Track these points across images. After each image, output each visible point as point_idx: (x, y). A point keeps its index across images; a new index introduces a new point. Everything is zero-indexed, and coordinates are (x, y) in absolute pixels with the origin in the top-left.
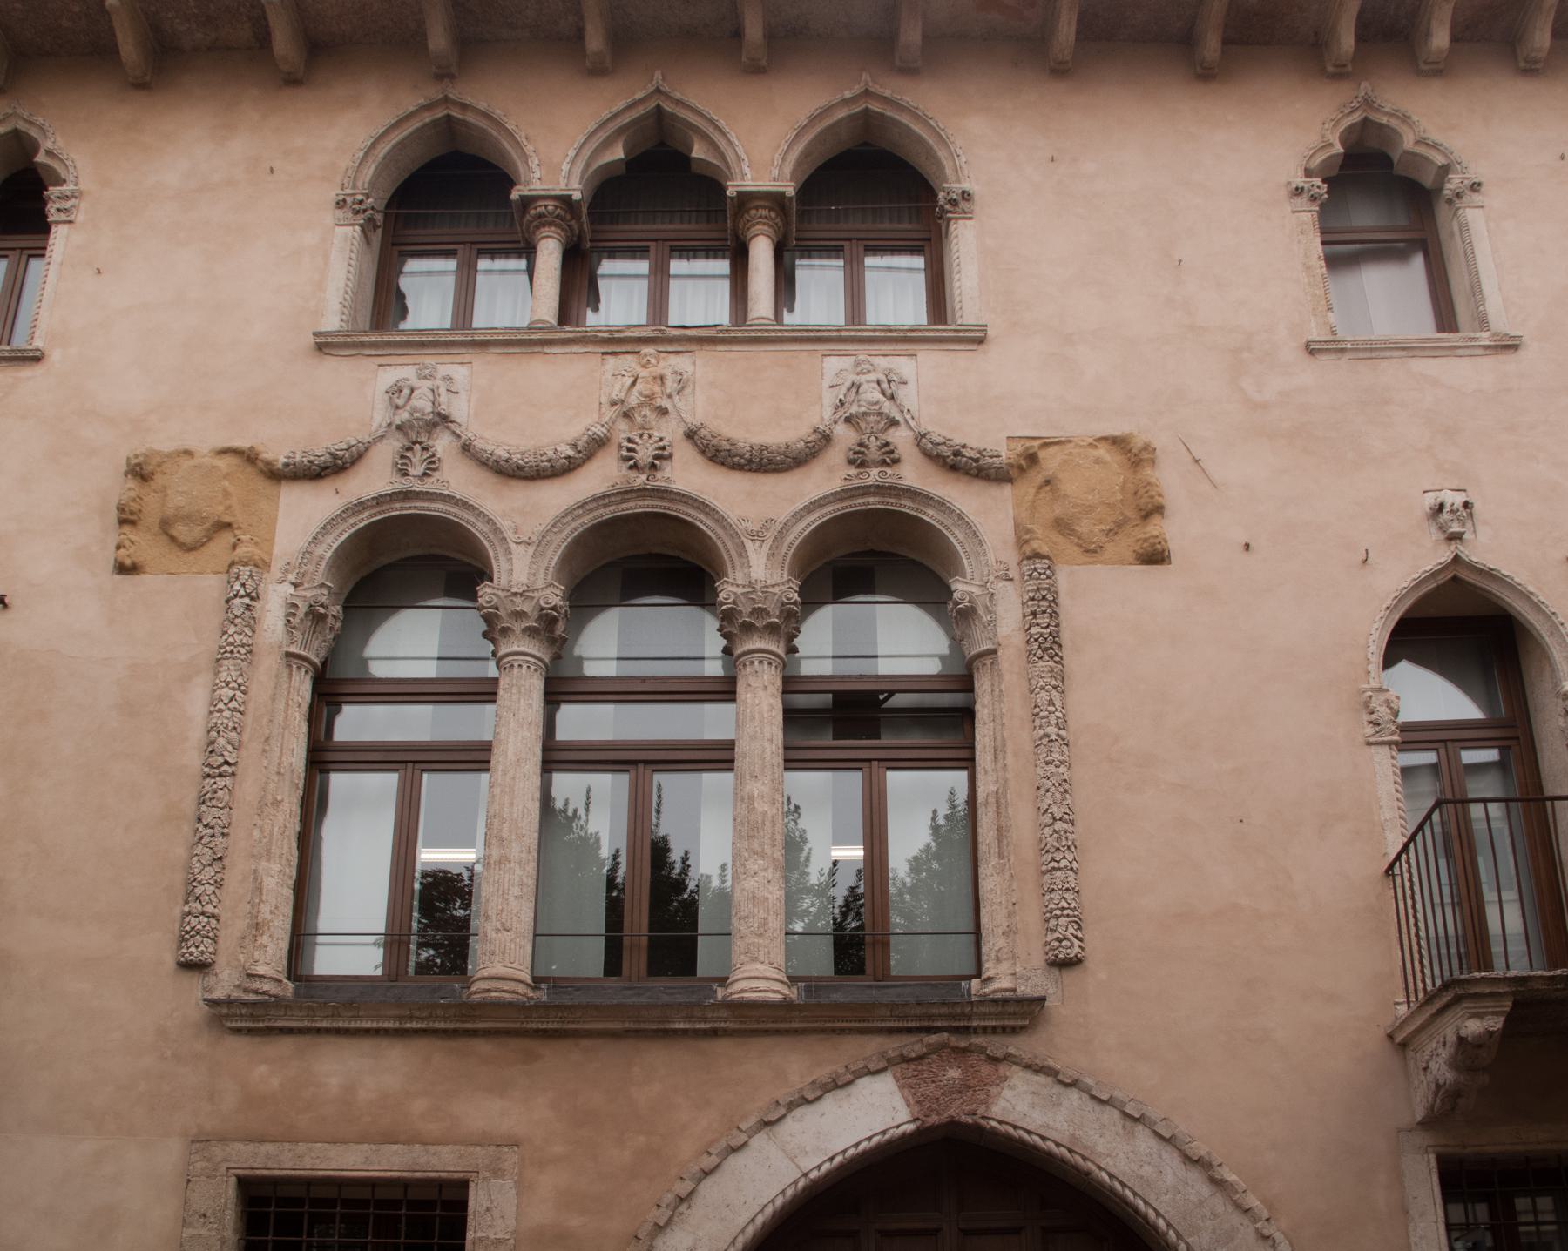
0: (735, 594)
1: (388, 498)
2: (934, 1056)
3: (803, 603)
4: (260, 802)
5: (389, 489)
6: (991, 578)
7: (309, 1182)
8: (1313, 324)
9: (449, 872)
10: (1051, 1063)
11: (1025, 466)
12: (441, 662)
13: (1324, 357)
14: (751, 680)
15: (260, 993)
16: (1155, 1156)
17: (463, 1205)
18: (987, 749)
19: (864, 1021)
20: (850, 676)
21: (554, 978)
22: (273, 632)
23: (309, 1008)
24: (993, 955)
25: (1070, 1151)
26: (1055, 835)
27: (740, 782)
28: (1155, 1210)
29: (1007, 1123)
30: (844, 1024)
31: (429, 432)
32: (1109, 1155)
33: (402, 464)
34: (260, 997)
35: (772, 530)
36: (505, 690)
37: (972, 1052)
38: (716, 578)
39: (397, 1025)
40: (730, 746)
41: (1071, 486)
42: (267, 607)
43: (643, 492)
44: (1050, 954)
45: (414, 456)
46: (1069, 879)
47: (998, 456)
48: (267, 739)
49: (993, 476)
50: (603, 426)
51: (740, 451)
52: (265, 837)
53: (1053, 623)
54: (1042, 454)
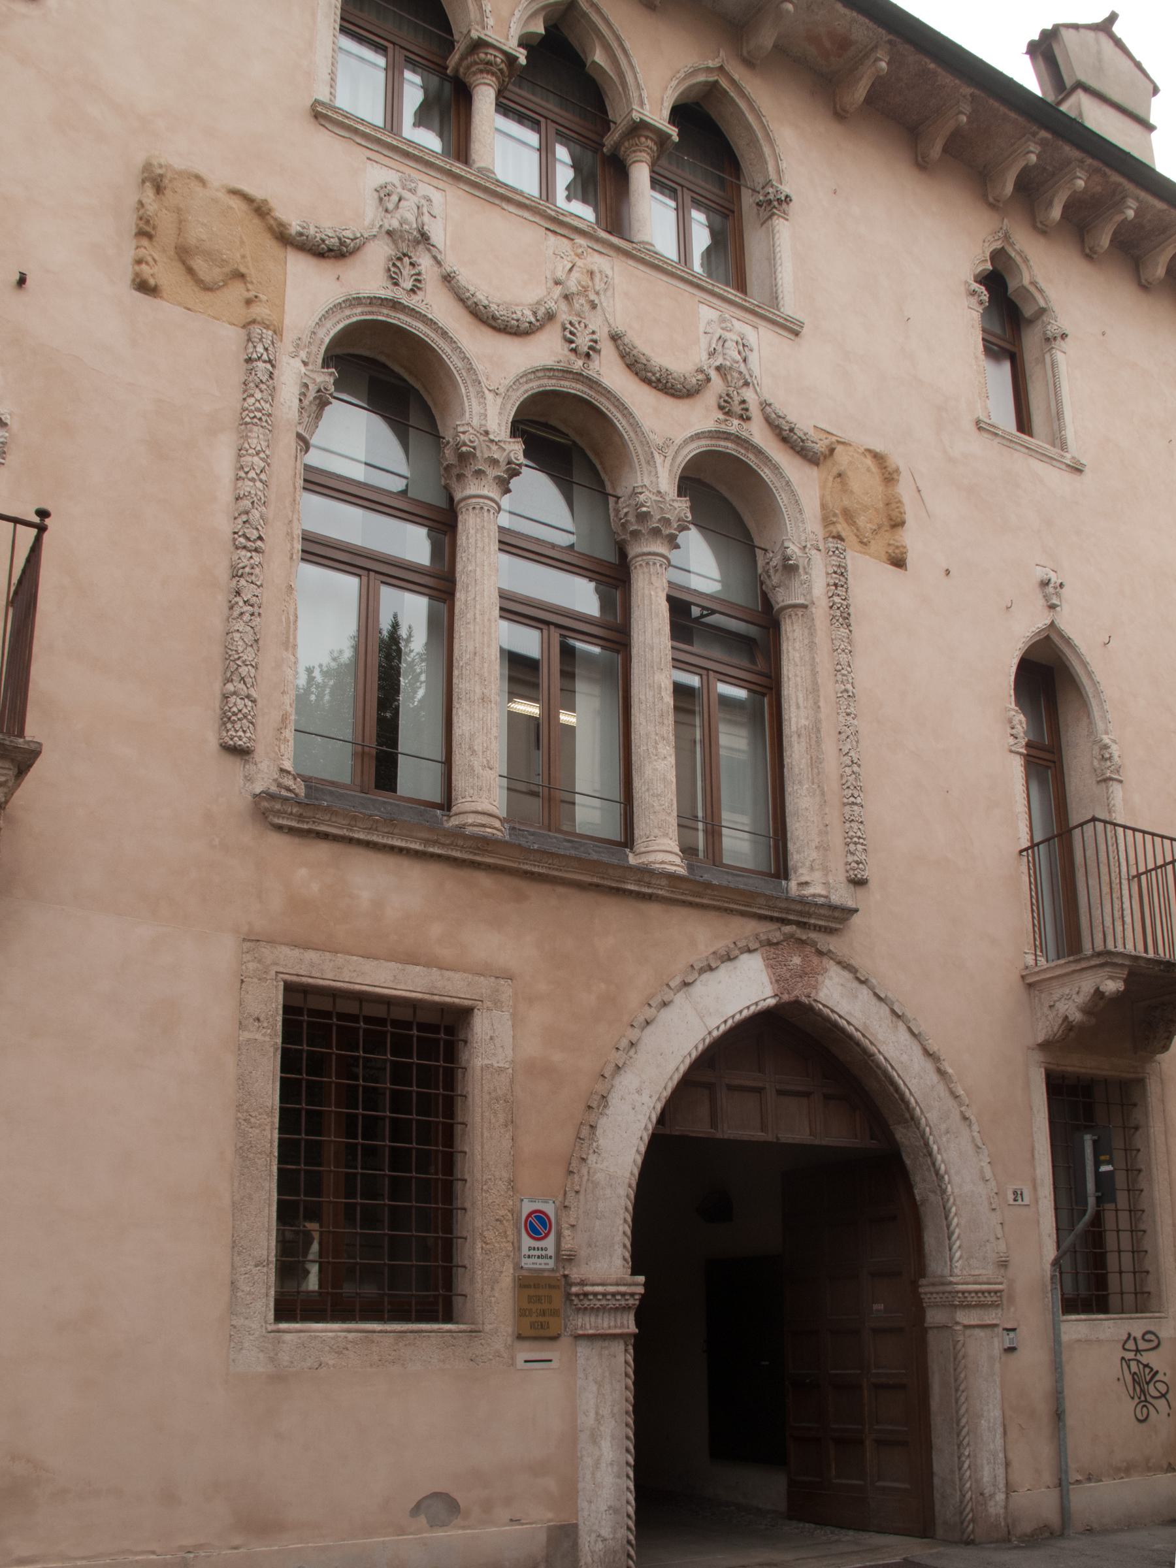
1: (380, 302)
2: (785, 944)
7: (334, 994)
8: (979, 406)
10: (852, 962)
13: (986, 435)
23: (354, 818)
24: (808, 864)
29: (828, 1007)
30: (735, 907)
32: (884, 1042)
45: (404, 267)
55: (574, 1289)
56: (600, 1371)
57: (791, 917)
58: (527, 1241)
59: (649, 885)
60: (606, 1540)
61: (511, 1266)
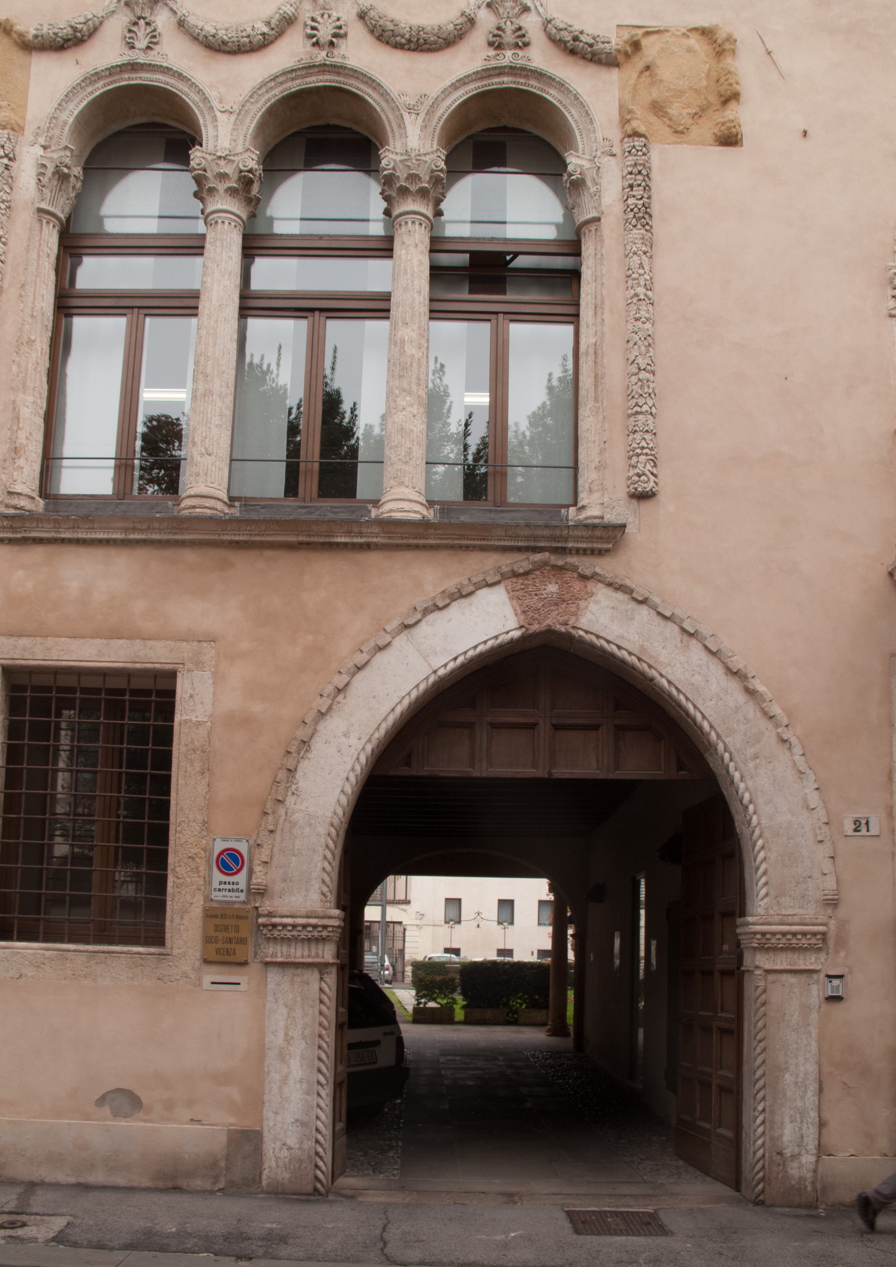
0: (394, 161)
1: (119, 69)
2: (538, 573)
3: (448, 172)
4: (17, 341)
5: (119, 61)
6: (599, 153)
7: (56, 672)
9: (170, 417)
10: (628, 582)
11: (630, 53)
12: (160, 219)
14: (406, 238)
15: (18, 509)
16: (704, 667)
17: (172, 693)
18: (590, 306)
19: (484, 540)
20: (484, 239)
21: (245, 498)
22: (27, 189)
23: (56, 521)
24: (587, 487)
25: (639, 659)
26: (640, 383)
27: (394, 328)
28: (702, 713)
29: (591, 633)
31: (152, 9)
32: (669, 665)
33: (130, 38)
34: (18, 512)
35: (425, 104)
36: (211, 243)
37: (567, 570)
38: (379, 147)
39: (123, 536)
40: (386, 297)
41: (665, 73)
42: (22, 167)
43: (323, 68)
44: (632, 487)
45: (139, 31)
46: (649, 422)
47: (609, 43)
48: (23, 285)
49: (604, 61)
50: (291, 5)
51: (402, 32)
52: (21, 372)
53: (646, 196)
54: (644, 42)
55: (261, 920)
56: (291, 996)
57: (542, 544)
58: (218, 876)
59: (361, 534)
60: (292, 1149)
61: (202, 898)
